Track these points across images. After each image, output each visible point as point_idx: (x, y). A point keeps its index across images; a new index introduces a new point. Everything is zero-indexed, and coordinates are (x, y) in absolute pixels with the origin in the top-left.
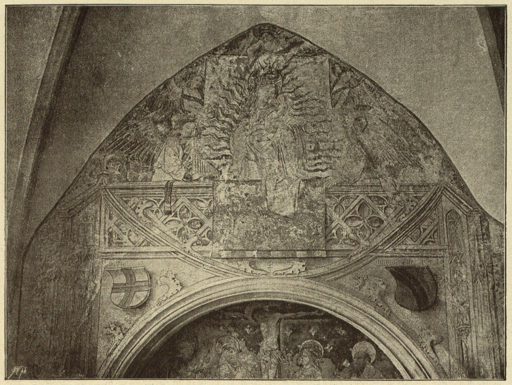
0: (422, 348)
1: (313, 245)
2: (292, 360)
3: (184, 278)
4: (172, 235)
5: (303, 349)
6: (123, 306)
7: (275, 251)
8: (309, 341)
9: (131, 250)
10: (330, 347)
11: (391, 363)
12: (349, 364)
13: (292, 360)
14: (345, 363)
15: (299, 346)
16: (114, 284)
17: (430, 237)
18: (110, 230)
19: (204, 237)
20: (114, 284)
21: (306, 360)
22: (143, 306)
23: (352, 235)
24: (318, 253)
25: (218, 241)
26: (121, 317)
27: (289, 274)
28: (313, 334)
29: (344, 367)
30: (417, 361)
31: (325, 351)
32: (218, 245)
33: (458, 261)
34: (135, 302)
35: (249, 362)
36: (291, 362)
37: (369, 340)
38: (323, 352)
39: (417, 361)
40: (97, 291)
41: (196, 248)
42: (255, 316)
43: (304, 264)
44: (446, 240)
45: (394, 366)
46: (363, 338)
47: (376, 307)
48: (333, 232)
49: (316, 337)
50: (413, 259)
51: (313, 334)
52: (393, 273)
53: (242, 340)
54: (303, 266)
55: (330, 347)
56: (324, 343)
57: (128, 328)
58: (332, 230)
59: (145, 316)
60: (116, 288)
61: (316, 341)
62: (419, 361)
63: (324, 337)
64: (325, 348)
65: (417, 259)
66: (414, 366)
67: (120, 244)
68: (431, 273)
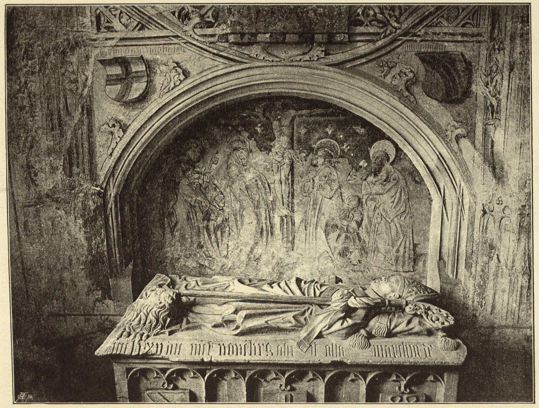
0: (447, 143)
1: (335, 26)
2: (306, 160)
3: (188, 66)
4: (171, 17)
5: (318, 148)
6: (121, 99)
7: (291, 34)
8: (324, 140)
9: (123, 35)
10: (347, 147)
11: (411, 162)
12: (366, 164)
13: (306, 160)
14: (361, 164)
15: (314, 146)
16: (108, 75)
17: (469, 19)
18: (98, 12)
19: (208, 17)
20: (108, 75)
21: (321, 161)
22: (143, 98)
23: (380, 16)
24: (340, 37)
25: (225, 22)
26: (121, 113)
27: (306, 61)
28: (330, 133)
29: (361, 167)
30: (440, 156)
31: (343, 151)
32: (225, 27)
33: (497, 47)
34: (135, 94)
35: (260, 163)
36: (304, 162)
37: (389, 139)
38: (339, 151)
39: (440, 156)
40: (89, 82)
41: (198, 31)
42: (268, 114)
43: (324, 49)
44: (486, 21)
45: (413, 165)
46: (382, 136)
47: (401, 98)
48: (358, 11)
49: (333, 137)
50: (446, 44)
51: (330, 133)
52: (423, 60)
53: (253, 139)
54: (322, 51)
55: (347, 147)
56: (341, 143)
57: (128, 124)
58: (358, 9)
59: (147, 110)
60: (110, 81)
61: (332, 140)
62: (442, 156)
63: (341, 137)
64: (342, 147)
65: (451, 44)
66: (435, 161)
67: (110, 29)
68: (465, 61)
